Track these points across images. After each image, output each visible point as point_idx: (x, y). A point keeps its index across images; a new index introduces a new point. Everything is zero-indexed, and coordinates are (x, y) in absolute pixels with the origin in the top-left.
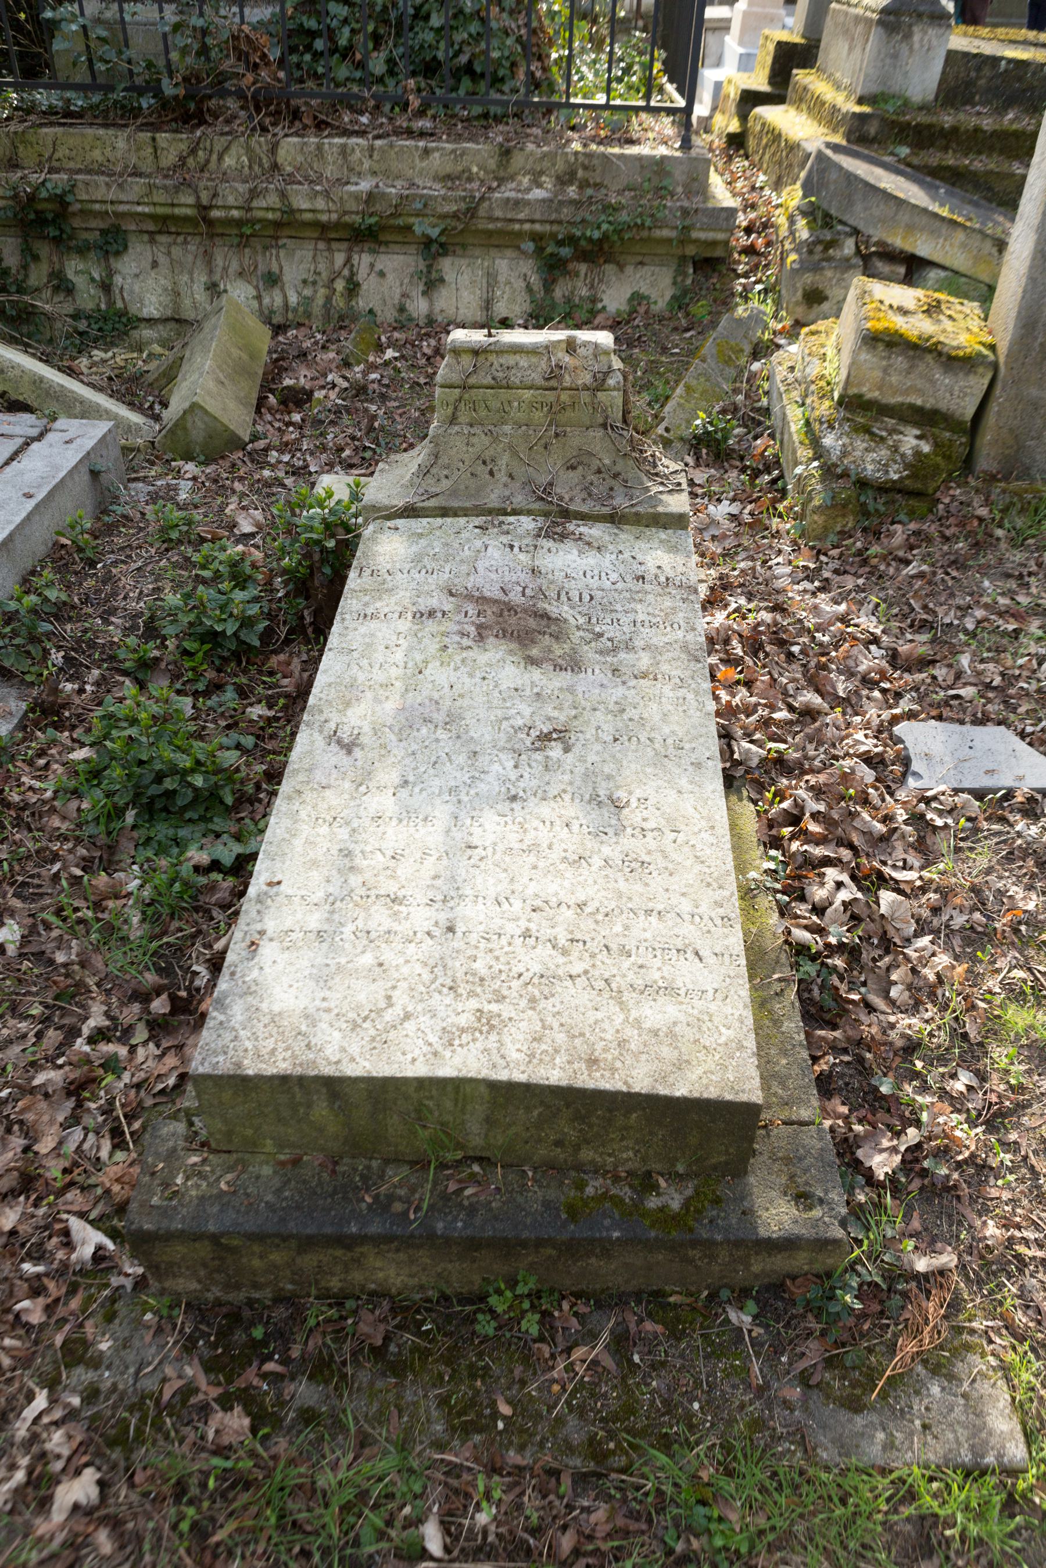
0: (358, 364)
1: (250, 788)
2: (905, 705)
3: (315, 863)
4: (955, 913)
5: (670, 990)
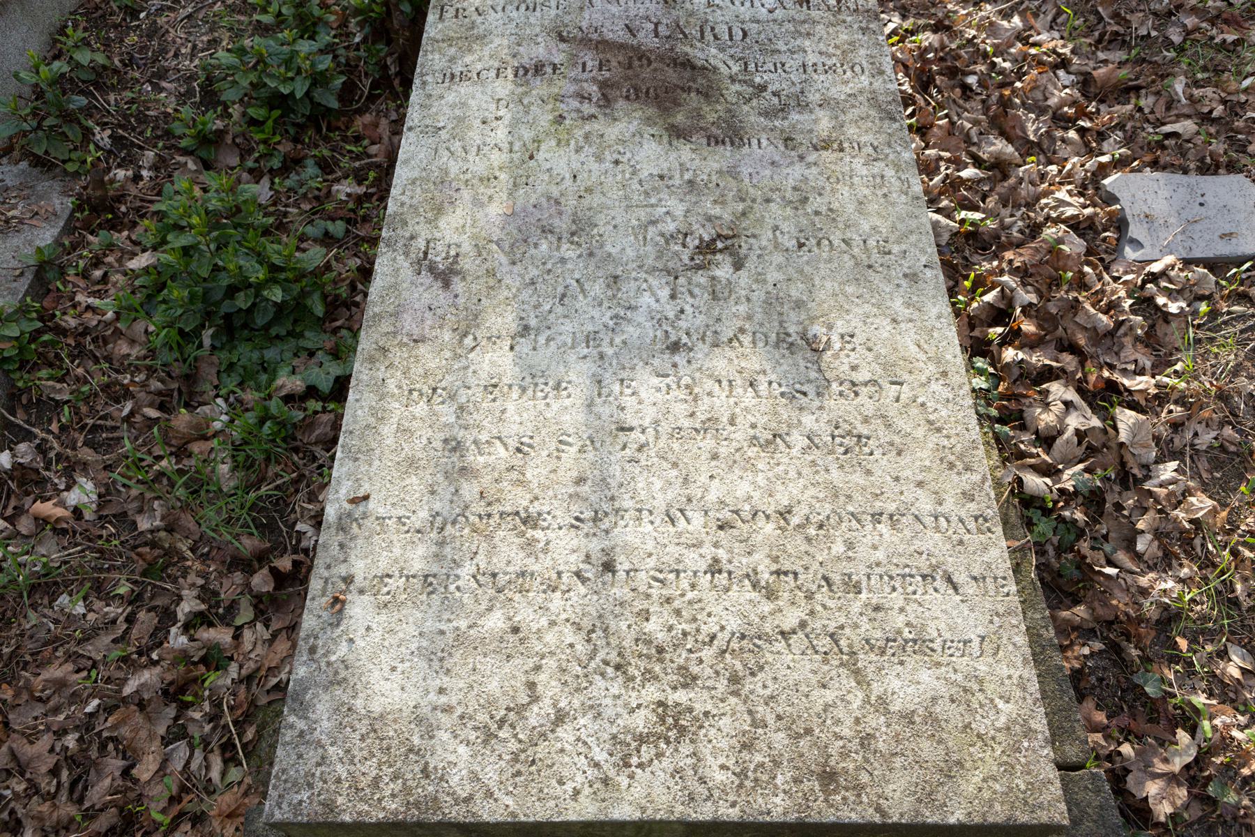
1: (343, 291)
2: (1113, 149)
3: (412, 464)
4: (1200, 428)
5: (920, 644)
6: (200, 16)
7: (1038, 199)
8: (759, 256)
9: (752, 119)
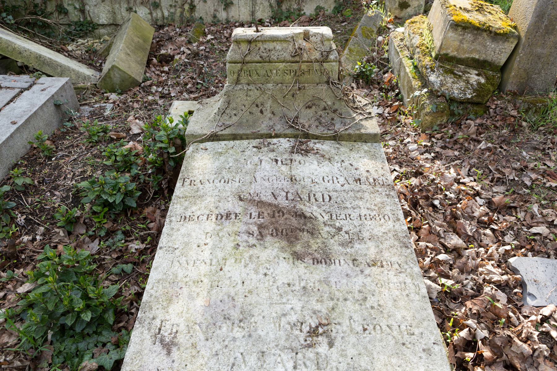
0: (195, 42)
6: (80, 160)
7: (477, 268)
8: (342, 338)
9: (336, 247)
